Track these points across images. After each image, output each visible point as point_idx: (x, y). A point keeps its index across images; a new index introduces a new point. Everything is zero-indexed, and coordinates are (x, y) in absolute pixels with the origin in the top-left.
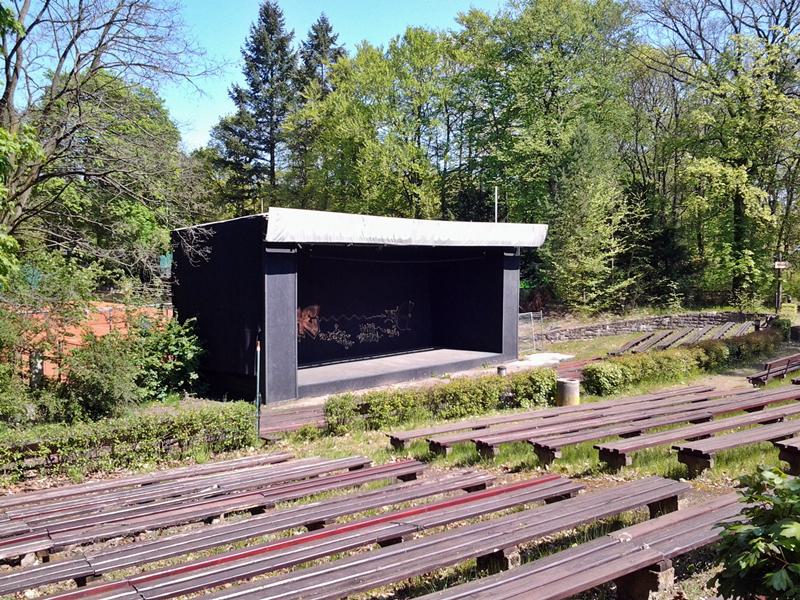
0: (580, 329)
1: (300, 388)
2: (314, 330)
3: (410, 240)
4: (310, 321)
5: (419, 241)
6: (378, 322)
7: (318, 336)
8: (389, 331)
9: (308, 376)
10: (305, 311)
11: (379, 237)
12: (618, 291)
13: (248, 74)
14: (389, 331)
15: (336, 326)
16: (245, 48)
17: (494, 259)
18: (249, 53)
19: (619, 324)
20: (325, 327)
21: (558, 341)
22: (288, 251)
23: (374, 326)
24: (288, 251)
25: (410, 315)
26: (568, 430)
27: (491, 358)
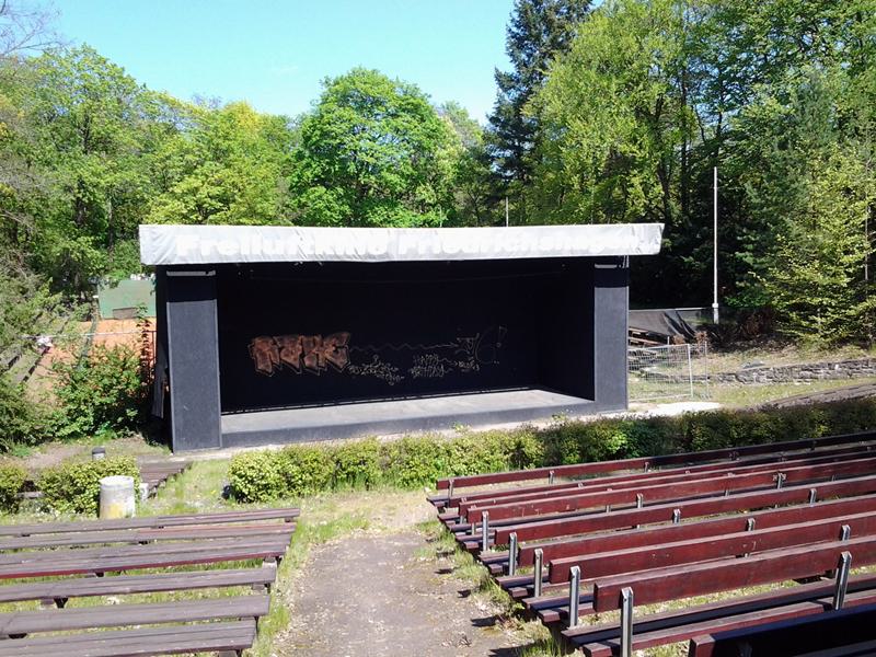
0: (791, 368)
1: (224, 435)
2: (341, 361)
3: (587, 251)
4: (336, 351)
5: (405, 256)
6: (441, 352)
7: (346, 370)
8: (461, 364)
9: (233, 423)
10: (328, 339)
11: (362, 252)
12: (862, 313)
13: (511, 55)
14: (461, 364)
15: (376, 358)
16: (510, 25)
17: (583, 273)
18: (514, 29)
19: (855, 363)
20: (354, 358)
21: (755, 384)
22: (203, 274)
23: (437, 358)
24: (203, 274)
25: (499, 345)
26: (132, 574)
27: (584, 405)
